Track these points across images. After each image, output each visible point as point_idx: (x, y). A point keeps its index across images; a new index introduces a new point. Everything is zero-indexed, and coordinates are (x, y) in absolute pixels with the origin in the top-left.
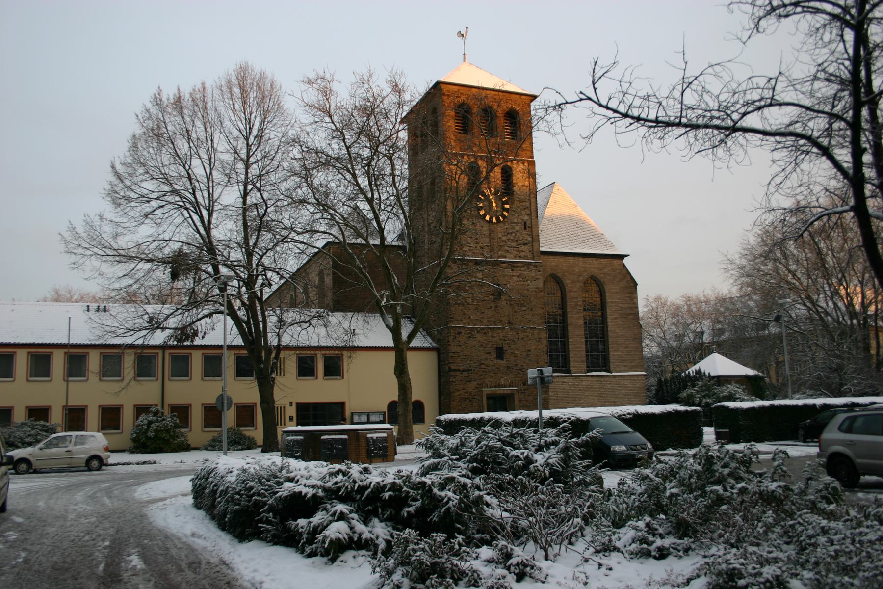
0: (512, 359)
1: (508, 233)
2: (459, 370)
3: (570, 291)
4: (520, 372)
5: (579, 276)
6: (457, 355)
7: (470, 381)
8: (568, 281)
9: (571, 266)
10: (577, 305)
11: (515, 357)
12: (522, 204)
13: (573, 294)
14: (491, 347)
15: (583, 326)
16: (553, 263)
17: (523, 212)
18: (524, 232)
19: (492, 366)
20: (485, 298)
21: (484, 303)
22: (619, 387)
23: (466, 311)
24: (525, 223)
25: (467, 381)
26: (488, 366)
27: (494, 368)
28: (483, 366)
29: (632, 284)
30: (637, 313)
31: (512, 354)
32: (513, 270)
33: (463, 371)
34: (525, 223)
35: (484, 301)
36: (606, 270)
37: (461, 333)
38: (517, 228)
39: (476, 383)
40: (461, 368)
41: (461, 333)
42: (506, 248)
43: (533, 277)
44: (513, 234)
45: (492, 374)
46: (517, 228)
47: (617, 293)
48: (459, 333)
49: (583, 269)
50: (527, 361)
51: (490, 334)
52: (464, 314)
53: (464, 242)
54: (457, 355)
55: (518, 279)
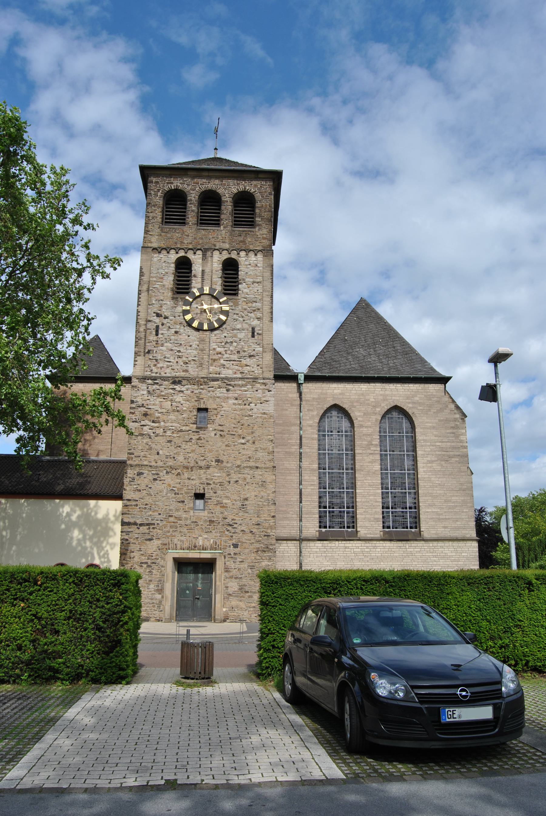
0: (218, 509)
1: (227, 343)
2: (135, 524)
3: (361, 426)
4: (230, 528)
5: (375, 407)
6: (134, 503)
7: (150, 540)
8: (357, 414)
9: (363, 394)
10: (370, 444)
11: (223, 507)
12: (250, 305)
13: (364, 430)
14: (186, 493)
15: (379, 472)
16: (335, 391)
17: (252, 315)
18: (253, 340)
19: (186, 519)
20: (184, 428)
21: (181, 433)
22: (435, 556)
23: (153, 446)
24: (253, 329)
25: (146, 540)
26: (180, 519)
27: (188, 522)
28: (171, 519)
29: (458, 416)
30: (48, 379)
31: (219, 503)
32: (228, 390)
33: (141, 525)
34: (253, 329)
35: (181, 431)
36: (416, 399)
37: (142, 474)
38: (241, 335)
39: (159, 542)
40: (139, 522)
41: (142, 474)
42: (222, 361)
43: (260, 399)
44: (235, 344)
45: (185, 530)
46: (241, 335)
47: (434, 428)
48: (139, 474)
49: (381, 397)
50: (241, 514)
51: (186, 475)
52: (150, 449)
53: (159, 357)
54: (134, 503)
55: (236, 402)
